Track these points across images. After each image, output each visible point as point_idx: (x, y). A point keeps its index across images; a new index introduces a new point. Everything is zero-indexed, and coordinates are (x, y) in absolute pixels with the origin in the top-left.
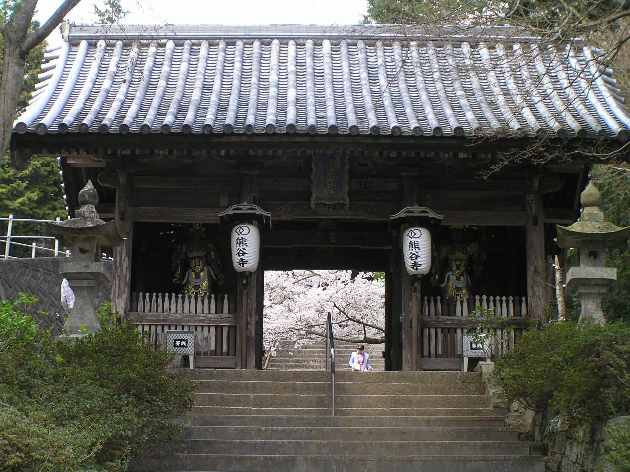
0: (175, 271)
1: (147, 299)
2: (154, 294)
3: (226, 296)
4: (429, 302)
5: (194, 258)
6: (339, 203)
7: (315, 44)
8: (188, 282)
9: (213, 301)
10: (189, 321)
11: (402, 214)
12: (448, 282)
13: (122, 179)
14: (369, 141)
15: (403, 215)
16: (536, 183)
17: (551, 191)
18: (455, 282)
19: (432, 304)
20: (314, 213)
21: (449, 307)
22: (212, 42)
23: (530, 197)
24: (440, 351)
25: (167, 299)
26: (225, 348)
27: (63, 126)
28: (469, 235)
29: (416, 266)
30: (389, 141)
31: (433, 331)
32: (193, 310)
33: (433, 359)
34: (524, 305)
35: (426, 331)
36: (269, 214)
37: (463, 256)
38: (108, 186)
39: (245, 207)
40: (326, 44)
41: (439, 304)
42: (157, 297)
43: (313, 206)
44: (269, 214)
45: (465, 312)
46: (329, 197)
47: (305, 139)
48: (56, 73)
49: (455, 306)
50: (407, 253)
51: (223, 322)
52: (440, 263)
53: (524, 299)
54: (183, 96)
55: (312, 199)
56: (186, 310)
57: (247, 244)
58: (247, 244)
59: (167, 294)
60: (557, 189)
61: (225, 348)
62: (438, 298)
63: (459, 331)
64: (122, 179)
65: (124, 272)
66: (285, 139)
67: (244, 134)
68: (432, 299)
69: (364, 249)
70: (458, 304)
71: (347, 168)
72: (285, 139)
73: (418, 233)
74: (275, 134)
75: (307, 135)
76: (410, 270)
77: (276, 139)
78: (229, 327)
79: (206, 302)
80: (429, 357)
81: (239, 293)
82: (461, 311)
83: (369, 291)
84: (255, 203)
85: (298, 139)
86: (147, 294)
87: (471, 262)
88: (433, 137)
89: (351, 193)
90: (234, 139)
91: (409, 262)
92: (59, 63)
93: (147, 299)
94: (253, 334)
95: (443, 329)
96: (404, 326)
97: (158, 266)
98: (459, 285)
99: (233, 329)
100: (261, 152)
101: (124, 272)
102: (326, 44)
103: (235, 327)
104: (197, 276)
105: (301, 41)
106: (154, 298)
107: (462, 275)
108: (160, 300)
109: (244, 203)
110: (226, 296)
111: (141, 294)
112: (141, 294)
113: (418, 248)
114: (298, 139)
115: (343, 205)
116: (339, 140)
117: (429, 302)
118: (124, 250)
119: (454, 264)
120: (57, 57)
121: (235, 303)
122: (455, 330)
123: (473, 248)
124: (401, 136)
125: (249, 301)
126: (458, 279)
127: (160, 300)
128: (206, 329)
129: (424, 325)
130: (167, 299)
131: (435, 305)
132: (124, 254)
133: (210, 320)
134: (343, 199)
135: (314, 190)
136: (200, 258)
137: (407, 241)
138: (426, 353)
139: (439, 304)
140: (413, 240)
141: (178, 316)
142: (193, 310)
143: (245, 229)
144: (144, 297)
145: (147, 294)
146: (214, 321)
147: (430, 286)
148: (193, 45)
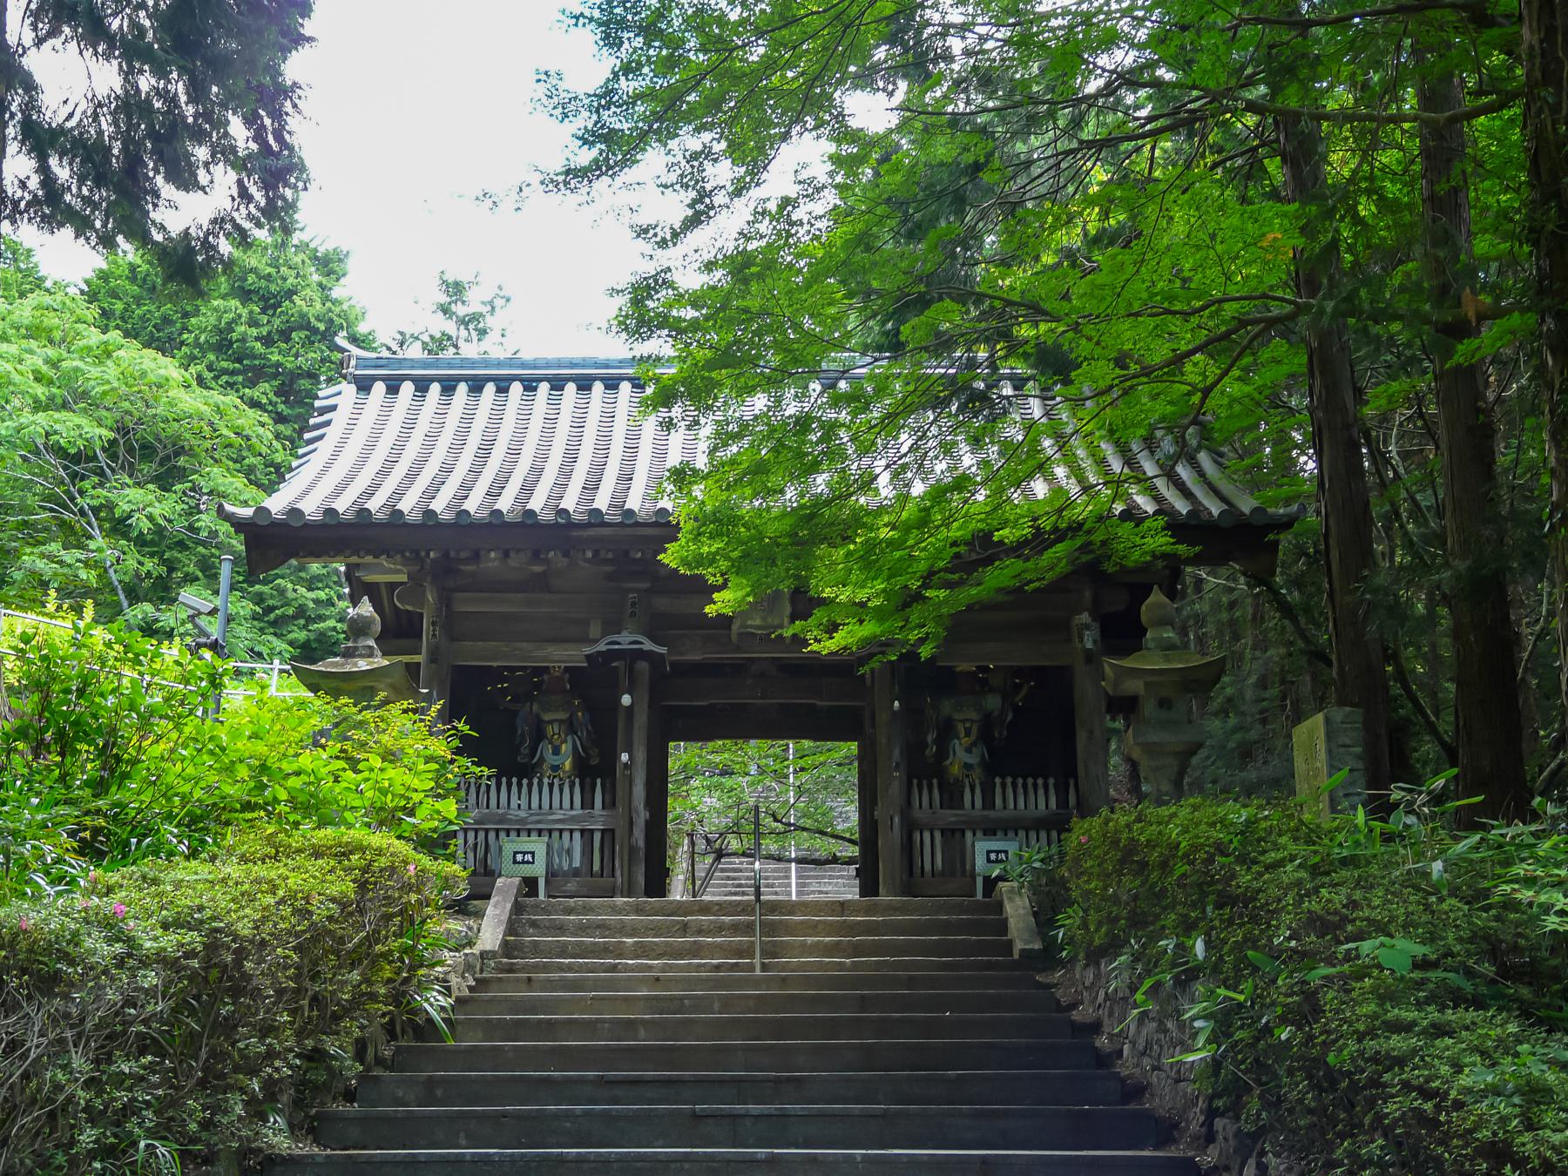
3: (599, 781)
5: (551, 722)
8: (542, 760)
19: (925, 792)
20: (738, 649)
21: (952, 797)
26: (596, 867)
31: (927, 835)
32: (546, 805)
34: (1072, 791)
35: (917, 836)
36: (663, 650)
37: (974, 716)
38: (409, 608)
44: (663, 650)
45: (978, 803)
53: (1072, 782)
56: (535, 804)
61: (596, 867)
63: (969, 834)
78: (603, 831)
82: (972, 800)
87: (987, 723)
90: (606, 531)
98: (970, 761)
103: (613, 831)
104: (556, 751)
107: (974, 744)
109: (625, 633)
110: (599, 781)
119: (961, 728)
129: (910, 827)
142: (546, 805)
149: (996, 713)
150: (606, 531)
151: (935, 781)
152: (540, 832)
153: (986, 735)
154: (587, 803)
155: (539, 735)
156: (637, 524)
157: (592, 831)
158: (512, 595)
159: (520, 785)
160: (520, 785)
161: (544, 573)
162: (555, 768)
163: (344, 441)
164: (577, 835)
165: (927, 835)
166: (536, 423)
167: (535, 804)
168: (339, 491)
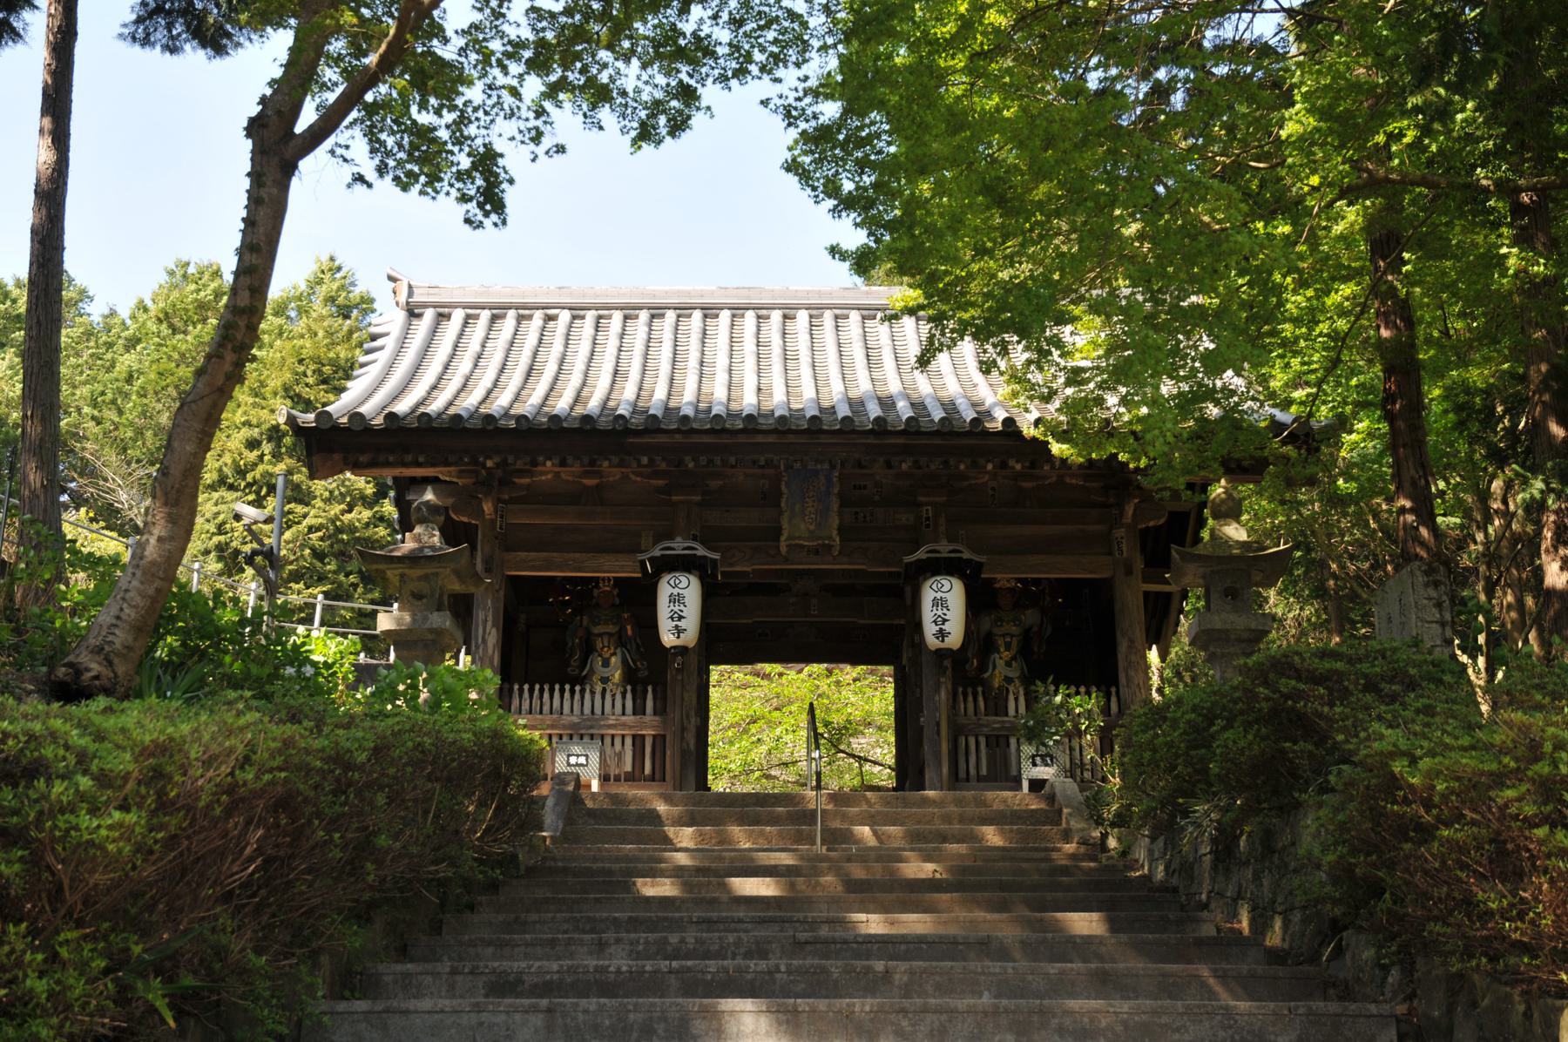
0: (571, 656)
1: (526, 694)
2: (537, 687)
3: (650, 689)
4: (965, 695)
5: (600, 635)
6: (823, 545)
7: (785, 317)
8: (592, 671)
9: (629, 696)
10: (591, 727)
11: (921, 554)
12: (994, 667)
13: (487, 507)
14: (871, 440)
15: (924, 556)
16: (1130, 510)
17: (1151, 524)
18: (1002, 668)
19: (970, 698)
20: (786, 560)
21: (997, 705)
22: (630, 312)
23: (1120, 533)
24: (984, 771)
25: (557, 694)
26: (648, 770)
27: (392, 417)
28: (1027, 595)
29: (942, 634)
30: (901, 441)
31: (972, 741)
32: (598, 710)
33: (973, 783)
34: (1114, 699)
35: (962, 740)
36: (716, 556)
37: (1014, 629)
38: (465, 519)
39: (679, 546)
40: (803, 316)
41: (981, 699)
42: (542, 691)
43: (784, 550)
44: (716, 556)
45: (1022, 709)
46: (807, 527)
47: (771, 439)
48: (382, 357)
49: (1007, 700)
50: (928, 614)
51: (645, 728)
52: (979, 640)
53: (1113, 690)
54: (584, 384)
55: (783, 538)
56: (587, 710)
57: (679, 610)
58: (679, 610)
59: (557, 687)
60: (1162, 521)
61: (648, 770)
62: (980, 689)
63: (1013, 741)
64: (487, 507)
65: (490, 651)
66: (742, 439)
67: (678, 431)
68: (970, 690)
69: (858, 624)
70: (1011, 697)
71: (836, 490)
72: (742, 439)
73: (947, 586)
74: (724, 431)
75: (774, 431)
76: (932, 641)
77: (726, 440)
78: (655, 737)
79: (618, 698)
80: (968, 780)
81: (671, 688)
82: (1016, 706)
83: (864, 696)
84: (695, 539)
85: (760, 439)
86: (526, 687)
87: (1026, 637)
88: (969, 434)
89: (840, 530)
90: (662, 439)
91: (930, 629)
92: (389, 343)
93: (526, 694)
94: (692, 747)
95: (987, 737)
96: (927, 733)
97: (545, 642)
98: (1010, 675)
99: (659, 740)
100: (703, 460)
101: (490, 651)
102: (803, 316)
103: (664, 737)
104: (606, 663)
105: (764, 312)
106: (536, 693)
107: (1014, 658)
108: (546, 695)
109: (679, 539)
110: (650, 689)
111: (516, 687)
112: (516, 687)
113: (944, 609)
114: (760, 439)
115: (830, 547)
116: (824, 439)
117: (965, 695)
118: (490, 618)
119: (1000, 641)
120: (387, 334)
121: (665, 699)
122: (1007, 738)
123: (1031, 617)
124: (919, 433)
125: (686, 695)
126: (1008, 664)
127: (546, 695)
128: (618, 741)
129: (957, 731)
130: (557, 694)
131: (975, 700)
132: (489, 624)
133: (624, 725)
134: (830, 538)
135: (785, 525)
136: (610, 635)
137: (928, 595)
138: (962, 774)
139: (981, 699)
140: (939, 595)
141: (575, 719)
142: (598, 710)
143: (683, 579)
144: (521, 691)
145: (526, 687)
146: (631, 728)
147: (965, 665)
148: (600, 317)
149: (1035, 629)
150: (662, 439)
151: (980, 689)
152: (592, 737)
153: (1025, 652)
154: (639, 710)
155: (589, 649)
156: (693, 431)
157: (643, 736)
158: (523, 554)
159: (572, 692)
160: (572, 692)
161: (597, 486)
162: (605, 680)
163: (391, 366)
164: (629, 741)
165: (972, 741)
166: (584, 348)
167: (587, 710)
168: (396, 396)
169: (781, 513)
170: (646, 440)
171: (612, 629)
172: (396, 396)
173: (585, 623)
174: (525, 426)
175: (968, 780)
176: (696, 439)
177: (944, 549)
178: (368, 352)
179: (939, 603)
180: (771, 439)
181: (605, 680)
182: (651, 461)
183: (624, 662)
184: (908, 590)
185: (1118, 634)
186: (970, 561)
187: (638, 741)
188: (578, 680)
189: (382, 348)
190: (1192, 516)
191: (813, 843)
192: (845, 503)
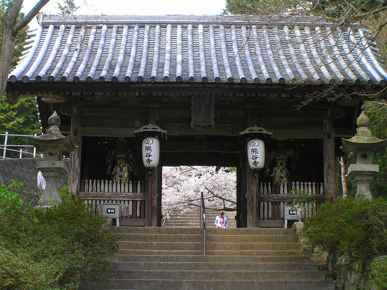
0: (108, 167)
1: (91, 184)
2: (95, 181)
3: (139, 182)
4: (263, 185)
5: (119, 158)
6: (208, 125)
8: (116, 173)
9: (131, 185)
10: (116, 197)
11: (247, 131)
13: (75, 110)
14: (227, 86)
15: (248, 132)
17: (338, 117)
18: (280, 173)
21: (276, 189)
22: (130, 26)
24: (270, 216)
25: (102, 184)
26: (138, 214)
27: (39, 77)
28: (288, 144)
31: (266, 204)
32: (119, 191)
36: (165, 132)
39: (150, 127)
40: (201, 27)
41: (270, 187)
42: (97, 182)
43: (192, 127)
44: (165, 132)
45: (286, 192)
46: (202, 121)
47: (188, 86)
50: (250, 155)
51: (137, 198)
52: (270, 162)
53: (322, 184)
55: (192, 122)
56: (114, 191)
57: (152, 150)
58: (152, 150)
59: (103, 181)
61: (138, 214)
62: (269, 183)
63: (282, 204)
65: (76, 167)
66: (175, 86)
67: (150, 82)
68: (265, 183)
69: (223, 153)
70: (282, 187)
71: (213, 103)
72: (175, 86)
76: (252, 166)
77: (169, 86)
78: (141, 201)
79: (127, 185)
81: (147, 180)
82: (283, 191)
84: (156, 124)
85: (183, 85)
87: (289, 161)
89: (215, 119)
90: (144, 85)
91: (251, 161)
92: (36, 39)
93: (91, 184)
94: (156, 205)
95: (272, 202)
96: (248, 200)
97: (97, 163)
99: (143, 202)
101: (76, 167)
103: (144, 201)
104: (121, 170)
105: (185, 25)
106: (95, 183)
107: (284, 169)
108: (98, 184)
109: (150, 125)
110: (139, 182)
111: (87, 181)
112: (87, 181)
114: (183, 85)
115: (211, 126)
116: (208, 86)
117: (263, 185)
118: (76, 154)
120: (35, 35)
121: (145, 186)
122: (280, 202)
123: (290, 153)
125: (153, 185)
126: (281, 171)
127: (98, 184)
129: (260, 200)
130: (102, 184)
131: (267, 188)
132: (76, 156)
133: (129, 197)
134: (210, 122)
136: (123, 158)
137: (250, 148)
138: (262, 217)
139: (270, 187)
140: (254, 147)
142: (119, 191)
143: (151, 140)
144: (89, 183)
145: (91, 181)
147: (264, 176)
148: (119, 27)
150: (144, 85)
169: (191, 112)
170: (137, 86)
171: (124, 156)
172: (40, 66)
173: (113, 153)
174: (89, 81)
175: (264, 219)
176: (158, 86)
177: (256, 129)
178: (28, 43)
179: (254, 151)
180: (188, 86)
181: (121, 177)
182: (139, 93)
183: (128, 169)
184: (242, 143)
185: (324, 162)
186: (266, 134)
187: (134, 202)
188: (109, 177)
189: (33, 41)
190: (357, 109)
191: (204, 255)
192: (217, 107)
